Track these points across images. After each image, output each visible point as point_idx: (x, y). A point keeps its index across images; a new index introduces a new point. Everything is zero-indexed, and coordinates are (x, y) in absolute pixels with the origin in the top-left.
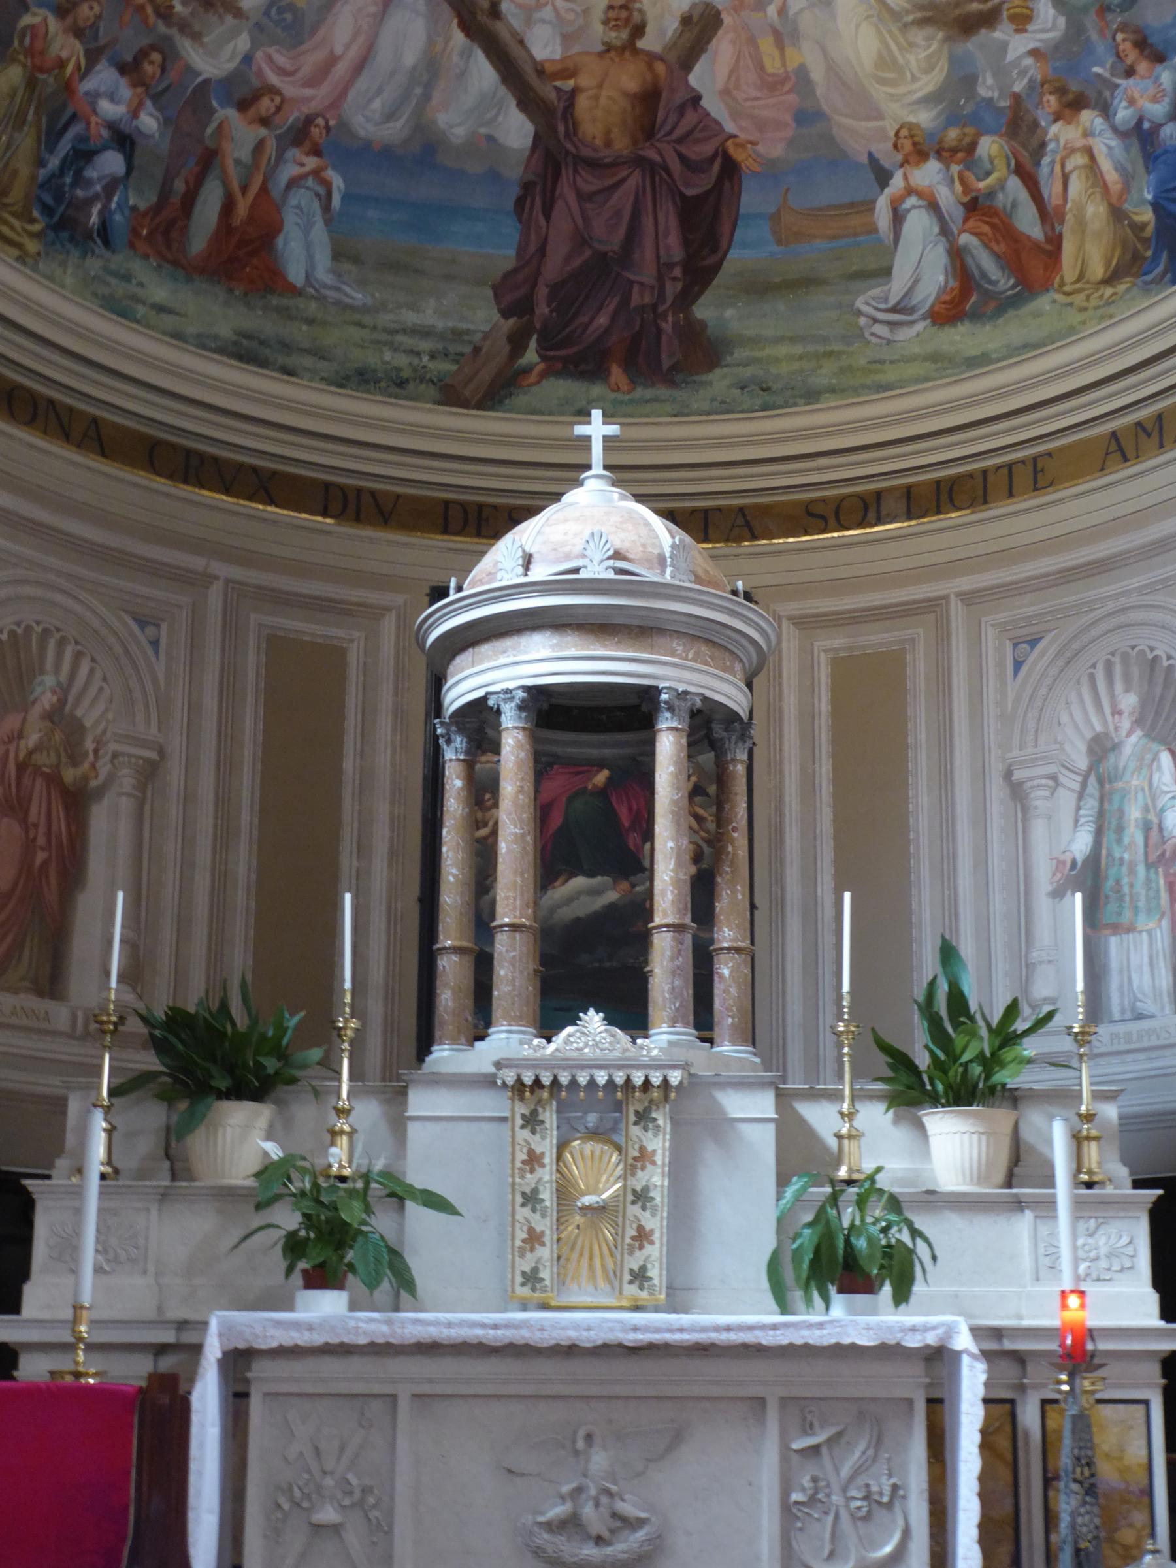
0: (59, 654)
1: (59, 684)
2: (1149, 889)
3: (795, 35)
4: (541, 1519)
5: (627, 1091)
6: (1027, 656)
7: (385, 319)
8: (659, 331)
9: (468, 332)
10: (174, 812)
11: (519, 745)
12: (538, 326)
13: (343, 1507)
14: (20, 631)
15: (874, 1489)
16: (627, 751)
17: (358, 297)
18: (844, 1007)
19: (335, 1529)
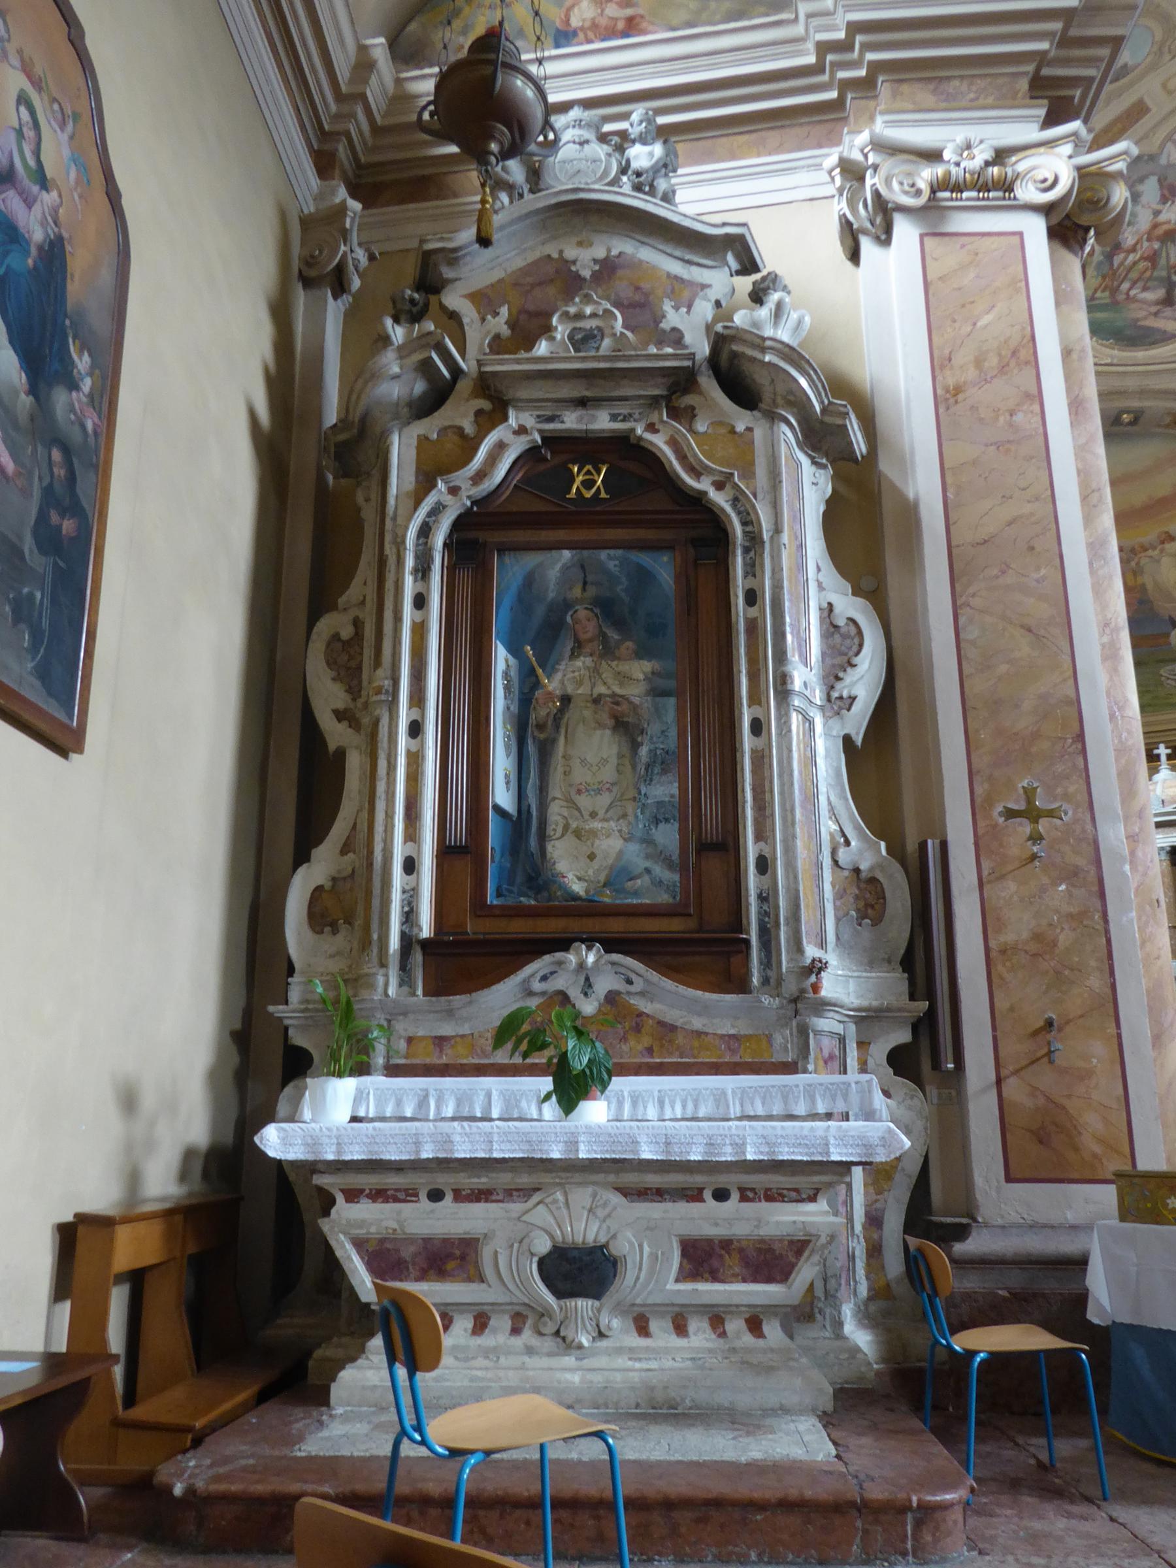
3: (1142, 572)
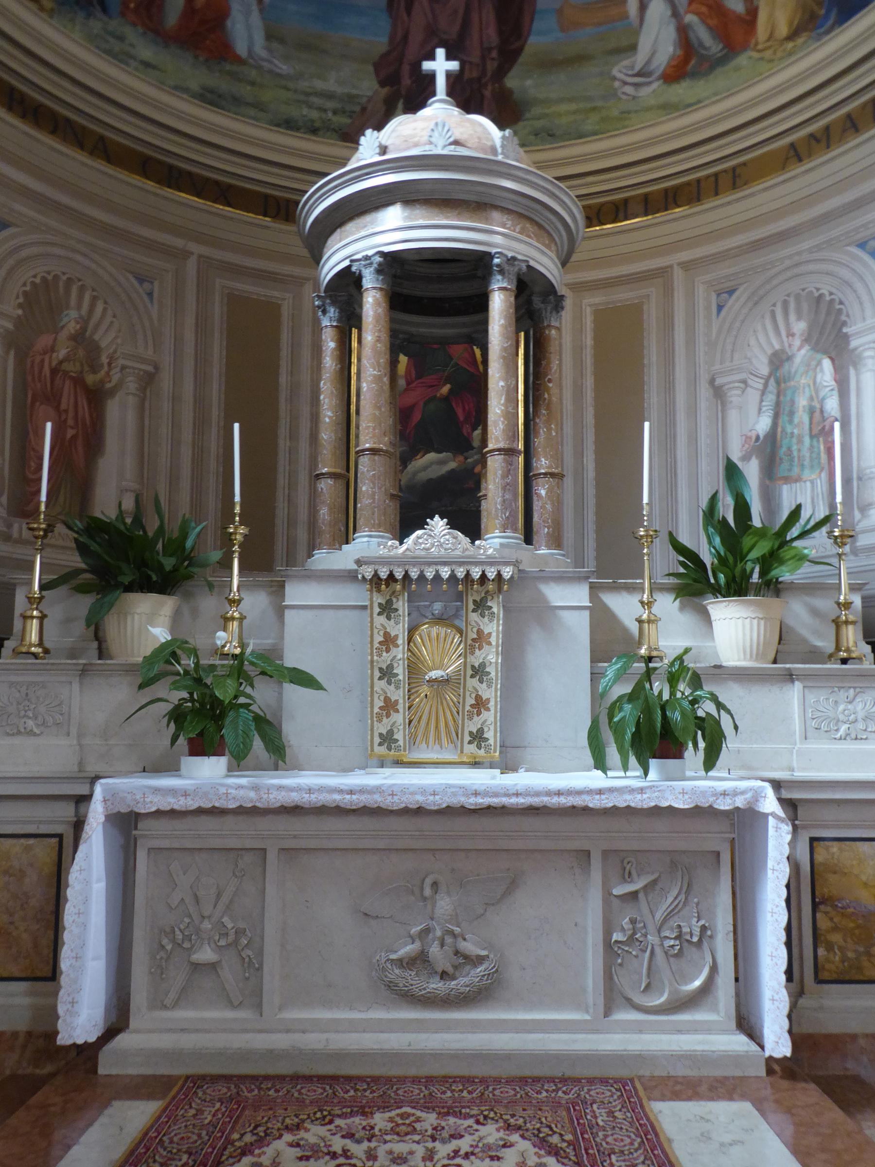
0: (80, 298)
1: (81, 317)
2: (812, 453)
4: (393, 956)
5: (467, 584)
6: (726, 301)
7: (303, 85)
8: (482, 96)
9: (358, 96)
10: (166, 406)
11: (377, 303)
12: (403, 92)
13: (220, 947)
14: (50, 278)
15: (686, 930)
16: (465, 330)
17: (284, 68)
18: (644, 515)
19: (213, 967)
